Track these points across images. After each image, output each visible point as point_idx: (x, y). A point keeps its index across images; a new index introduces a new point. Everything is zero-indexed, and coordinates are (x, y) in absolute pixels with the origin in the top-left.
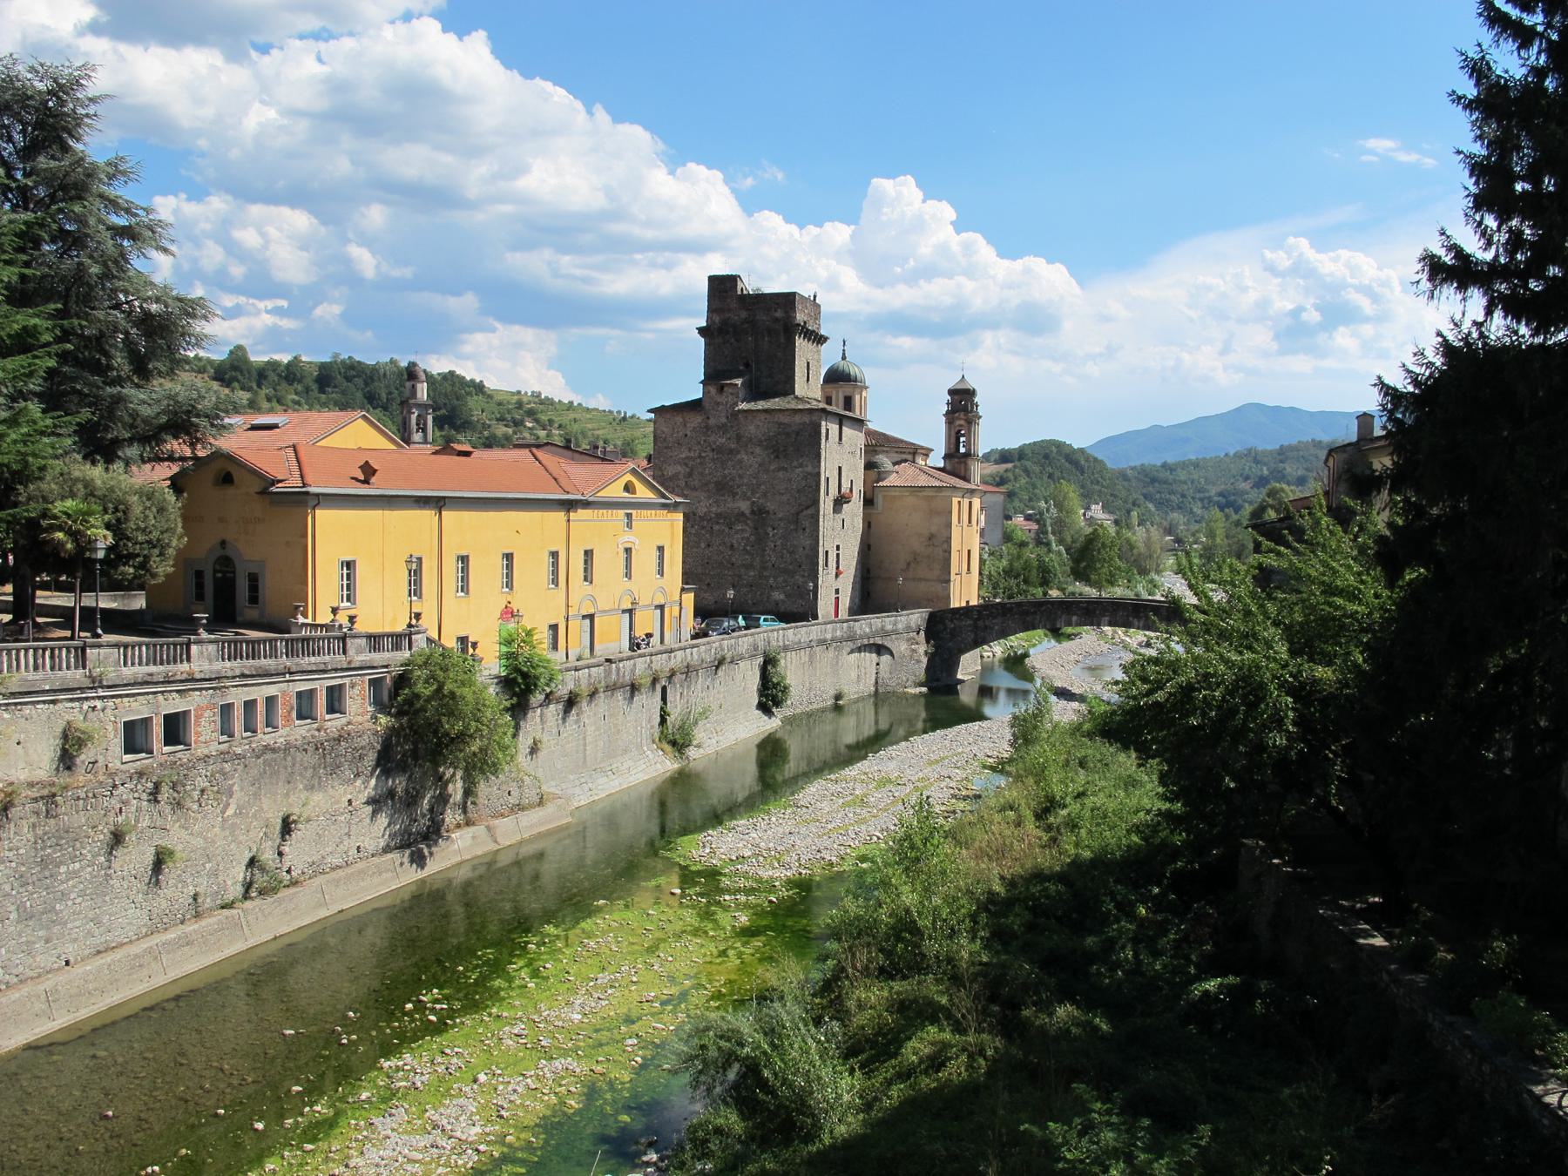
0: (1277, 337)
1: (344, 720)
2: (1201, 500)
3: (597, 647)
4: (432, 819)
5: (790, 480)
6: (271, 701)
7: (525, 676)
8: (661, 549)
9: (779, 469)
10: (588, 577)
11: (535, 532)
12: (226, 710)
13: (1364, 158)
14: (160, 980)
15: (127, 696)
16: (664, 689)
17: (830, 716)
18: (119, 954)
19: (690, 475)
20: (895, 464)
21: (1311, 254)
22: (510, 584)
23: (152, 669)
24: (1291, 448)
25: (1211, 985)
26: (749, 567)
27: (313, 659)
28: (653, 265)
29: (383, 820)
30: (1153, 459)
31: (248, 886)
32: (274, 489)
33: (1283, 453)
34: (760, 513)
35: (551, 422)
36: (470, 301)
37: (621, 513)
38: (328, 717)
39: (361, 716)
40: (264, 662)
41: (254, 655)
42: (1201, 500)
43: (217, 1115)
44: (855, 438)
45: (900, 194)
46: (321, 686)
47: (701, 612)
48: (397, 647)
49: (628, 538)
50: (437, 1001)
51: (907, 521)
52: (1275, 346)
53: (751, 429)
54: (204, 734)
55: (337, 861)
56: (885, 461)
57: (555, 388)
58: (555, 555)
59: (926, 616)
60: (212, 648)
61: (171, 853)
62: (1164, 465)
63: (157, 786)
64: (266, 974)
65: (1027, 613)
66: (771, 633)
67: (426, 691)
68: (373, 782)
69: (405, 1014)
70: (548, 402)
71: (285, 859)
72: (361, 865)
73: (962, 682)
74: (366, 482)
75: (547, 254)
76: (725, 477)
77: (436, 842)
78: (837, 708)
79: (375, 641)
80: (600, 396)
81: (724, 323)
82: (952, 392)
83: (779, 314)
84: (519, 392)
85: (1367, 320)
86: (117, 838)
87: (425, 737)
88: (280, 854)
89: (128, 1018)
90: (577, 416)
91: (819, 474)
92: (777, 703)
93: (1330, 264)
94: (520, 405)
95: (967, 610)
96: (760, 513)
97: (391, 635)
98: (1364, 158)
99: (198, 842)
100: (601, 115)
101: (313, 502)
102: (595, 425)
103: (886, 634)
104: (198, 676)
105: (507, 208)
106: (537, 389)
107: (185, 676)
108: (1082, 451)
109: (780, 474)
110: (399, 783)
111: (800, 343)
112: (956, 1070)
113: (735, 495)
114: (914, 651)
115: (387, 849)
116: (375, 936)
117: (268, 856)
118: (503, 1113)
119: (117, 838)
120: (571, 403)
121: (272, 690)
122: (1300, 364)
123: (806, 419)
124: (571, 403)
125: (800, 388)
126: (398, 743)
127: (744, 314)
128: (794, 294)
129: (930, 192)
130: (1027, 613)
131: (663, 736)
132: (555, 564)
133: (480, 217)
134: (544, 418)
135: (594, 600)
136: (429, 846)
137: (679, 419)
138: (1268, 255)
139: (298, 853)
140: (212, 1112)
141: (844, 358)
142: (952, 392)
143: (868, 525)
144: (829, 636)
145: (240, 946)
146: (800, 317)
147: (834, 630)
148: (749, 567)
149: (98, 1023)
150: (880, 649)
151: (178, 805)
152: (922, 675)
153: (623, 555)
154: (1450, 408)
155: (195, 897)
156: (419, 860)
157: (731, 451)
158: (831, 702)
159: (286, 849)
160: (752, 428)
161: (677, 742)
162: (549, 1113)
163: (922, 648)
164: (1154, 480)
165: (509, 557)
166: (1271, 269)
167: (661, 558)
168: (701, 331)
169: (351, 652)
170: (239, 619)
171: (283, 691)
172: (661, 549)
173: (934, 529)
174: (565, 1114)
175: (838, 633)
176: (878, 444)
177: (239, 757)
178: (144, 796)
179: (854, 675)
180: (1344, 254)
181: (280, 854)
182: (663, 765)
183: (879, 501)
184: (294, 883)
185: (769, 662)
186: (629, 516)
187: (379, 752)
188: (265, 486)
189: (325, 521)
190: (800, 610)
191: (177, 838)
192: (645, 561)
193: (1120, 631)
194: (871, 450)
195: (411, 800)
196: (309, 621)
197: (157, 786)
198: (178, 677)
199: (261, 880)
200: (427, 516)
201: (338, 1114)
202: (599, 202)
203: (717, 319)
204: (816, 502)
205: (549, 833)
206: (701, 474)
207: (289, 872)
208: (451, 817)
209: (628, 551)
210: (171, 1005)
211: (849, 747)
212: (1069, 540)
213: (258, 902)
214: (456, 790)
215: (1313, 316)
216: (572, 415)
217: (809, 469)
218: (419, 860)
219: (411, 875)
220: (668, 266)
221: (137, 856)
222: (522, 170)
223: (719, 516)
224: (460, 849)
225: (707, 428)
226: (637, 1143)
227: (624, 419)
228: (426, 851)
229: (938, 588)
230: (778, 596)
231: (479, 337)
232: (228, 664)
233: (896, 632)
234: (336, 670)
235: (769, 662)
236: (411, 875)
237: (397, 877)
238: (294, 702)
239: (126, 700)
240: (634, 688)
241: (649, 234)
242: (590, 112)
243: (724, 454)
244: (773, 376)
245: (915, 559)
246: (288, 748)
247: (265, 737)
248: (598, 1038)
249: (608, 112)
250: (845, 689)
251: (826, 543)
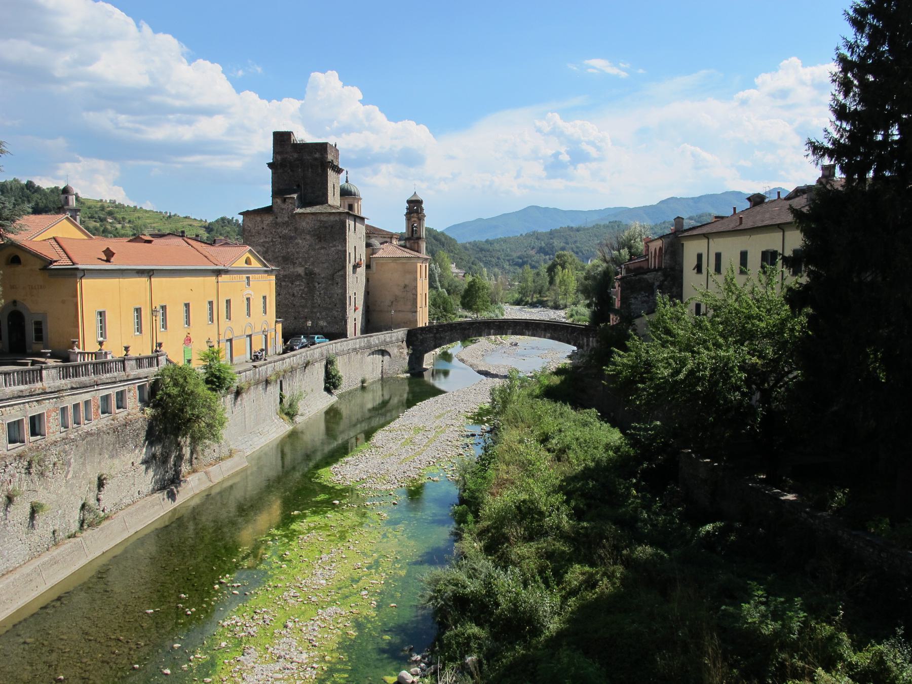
0: (546, 168)
1: (126, 413)
2: (508, 261)
3: (235, 358)
4: (175, 471)
5: (328, 255)
6: (87, 403)
7: (218, 378)
8: (265, 298)
10: (229, 317)
11: (200, 289)
12: (64, 410)
13: (590, 71)
14: (43, 589)
15: (9, 406)
16: (281, 382)
17: (359, 393)
18: (16, 575)
20: (381, 244)
21: (560, 123)
22: (188, 322)
23: (22, 387)
24: (556, 231)
25: (709, 527)
27: (108, 375)
28: (180, 122)
29: (151, 473)
30: (481, 238)
31: (82, 523)
32: (52, 267)
33: (552, 234)
34: (310, 274)
35: (123, 218)
36: (61, 142)
37: (245, 276)
38: (117, 411)
39: (135, 411)
40: (84, 379)
41: (76, 375)
42: (508, 261)
43: (134, 669)
44: (361, 229)
45: (328, 82)
46: (112, 392)
47: (286, 337)
48: (151, 365)
49: (248, 292)
50: (232, 581)
51: (391, 278)
52: (544, 174)
53: (304, 224)
54: (52, 428)
55: (127, 501)
56: (375, 242)
57: (120, 197)
58: (211, 303)
59: (406, 332)
60: (54, 371)
61: (42, 506)
62: (487, 241)
63: (30, 463)
64: (98, 580)
65: (465, 329)
66: (324, 347)
67: (174, 391)
68: (144, 450)
69: (217, 591)
70: (121, 207)
71: (102, 502)
72: (142, 502)
73: (426, 370)
74: (108, 261)
75: (111, 114)
76: (288, 253)
77: (179, 484)
78: (363, 388)
79: (139, 361)
80: (148, 202)
81: (284, 160)
82: (409, 202)
83: (317, 155)
84: (101, 201)
85: (595, 160)
86: (10, 499)
87: (173, 418)
88: (98, 500)
89: (33, 615)
90: (140, 215)
91: (345, 251)
92: (335, 387)
93: (575, 128)
94: (103, 208)
95: (422, 329)
96: (310, 274)
97: (147, 358)
98: (590, 71)
99: (53, 497)
100: (146, 28)
101: (80, 274)
102: (151, 221)
103: (387, 343)
104: (48, 390)
105: (81, 84)
106: (113, 198)
107: (41, 391)
108: (442, 233)
109: (322, 251)
110: (158, 449)
111: (331, 173)
112: (604, 586)
113: (294, 264)
114: (401, 353)
115: (154, 491)
116: (152, 548)
117: (92, 502)
118: (314, 643)
119: (10, 499)
120: (135, 207)
121: (87, 397)
122: (558, 184)
123: (337, 218)
124: (135, 207)
125: (331, 201)
126: (157, 425)
127: (296, 155)
128: (326, 144)
129: (346, 80)
130: (465, 329)
131: (282, 410)
132: (211, 309)
133: (65, 89)
134: (119, 216)
135: (232, 330)
136: (176, 487)
137: (259, 219)
138: (538, 123)
139: (108, 498)
140: (131, 667)
141: (347, 182)
142: (409, 202)
143: (368, 280)
144: (358, 346)
145: (83, 562)
146: (330, 157)
147: (360, 343)
148: (304, 307)
149: (16, 621)
150: (383, 353)
151: (42, 474)
152: (406, 367)
153: (262, 300)
154: (818, 211)
155: (54, 532)
156: (172, 496)
157: (291, 238)
158: (360, 385)
159: (101, 497)
160: (304, 224)
161: (290, 413)
162: (341, 640)
163: (405, 351)
164: (482, 250)
165: (187, 305)
166: (539, 130)
167: (265, 303)
168: (270, 165)
169: (128, 369)
170: (28, 351)
171: (94, 396)
172: (265, 298)
173: (407, 282)
174: (351, 640)
175: (362, 344)
176: (372, 232)
177: (73, 440)
178: (23, 471)
179: (370, 369)
180: (578, 122)
181: (98, 500)
182: (283, 428)
183: (374, 265)
184: (107, 518)
185: (329, 362)
186: (248, 278)
187: (147, 431)
188: (46, 264)
189: (87, 285)
190: (337, 333)
191: (41, 497)
192: (257, 305)
193: (499, 337)
194: (368, 236)
195: (165, 460)
196: (81, 350)
197: (30, 463)
198: (37, 392)
199: (89, 517)
200: (144, 280)
201: (212, 657)
202: (144, 81)
203: (279, 158)
204: (344, 267)
205: (237, 473)
206: (274, 252)
207: (103, 511)
208: (185, 468)
209: (248, 299)
210: (58, 604)
211: (370, 410)
212: (447, 285)
213: (89, 531)
214: (187, 451)
215: (565, 158)
216: (137, 215)
217: (340, 248)
218: (172, 496)
219: (169, 506)
220: (190, 123)
221: (21, 510)
222: (93, 59)
224: (193, 486)
225: (276, 224)
226: (403, 650)
227: (170, 217)
228: (175, 490)
229: (410, 316)
231: (69, 165)
232: (63, 381)
233: (391, 342)
234: (121, 381)
235: (329, 362)
236: (169, 506)
237: (160, 508)
238: (100, 403)
239: (8, 409)
240: (267, 382)
241: (178, 103)
242: (138, 26)
243: (288, 240)
244: (315, 194)
245: (396, 299)
246: (99, 433)
247: (85, 427)
248: (344, 591)
249: (151, 27)
250: (367, 377)
251: (350, 292)
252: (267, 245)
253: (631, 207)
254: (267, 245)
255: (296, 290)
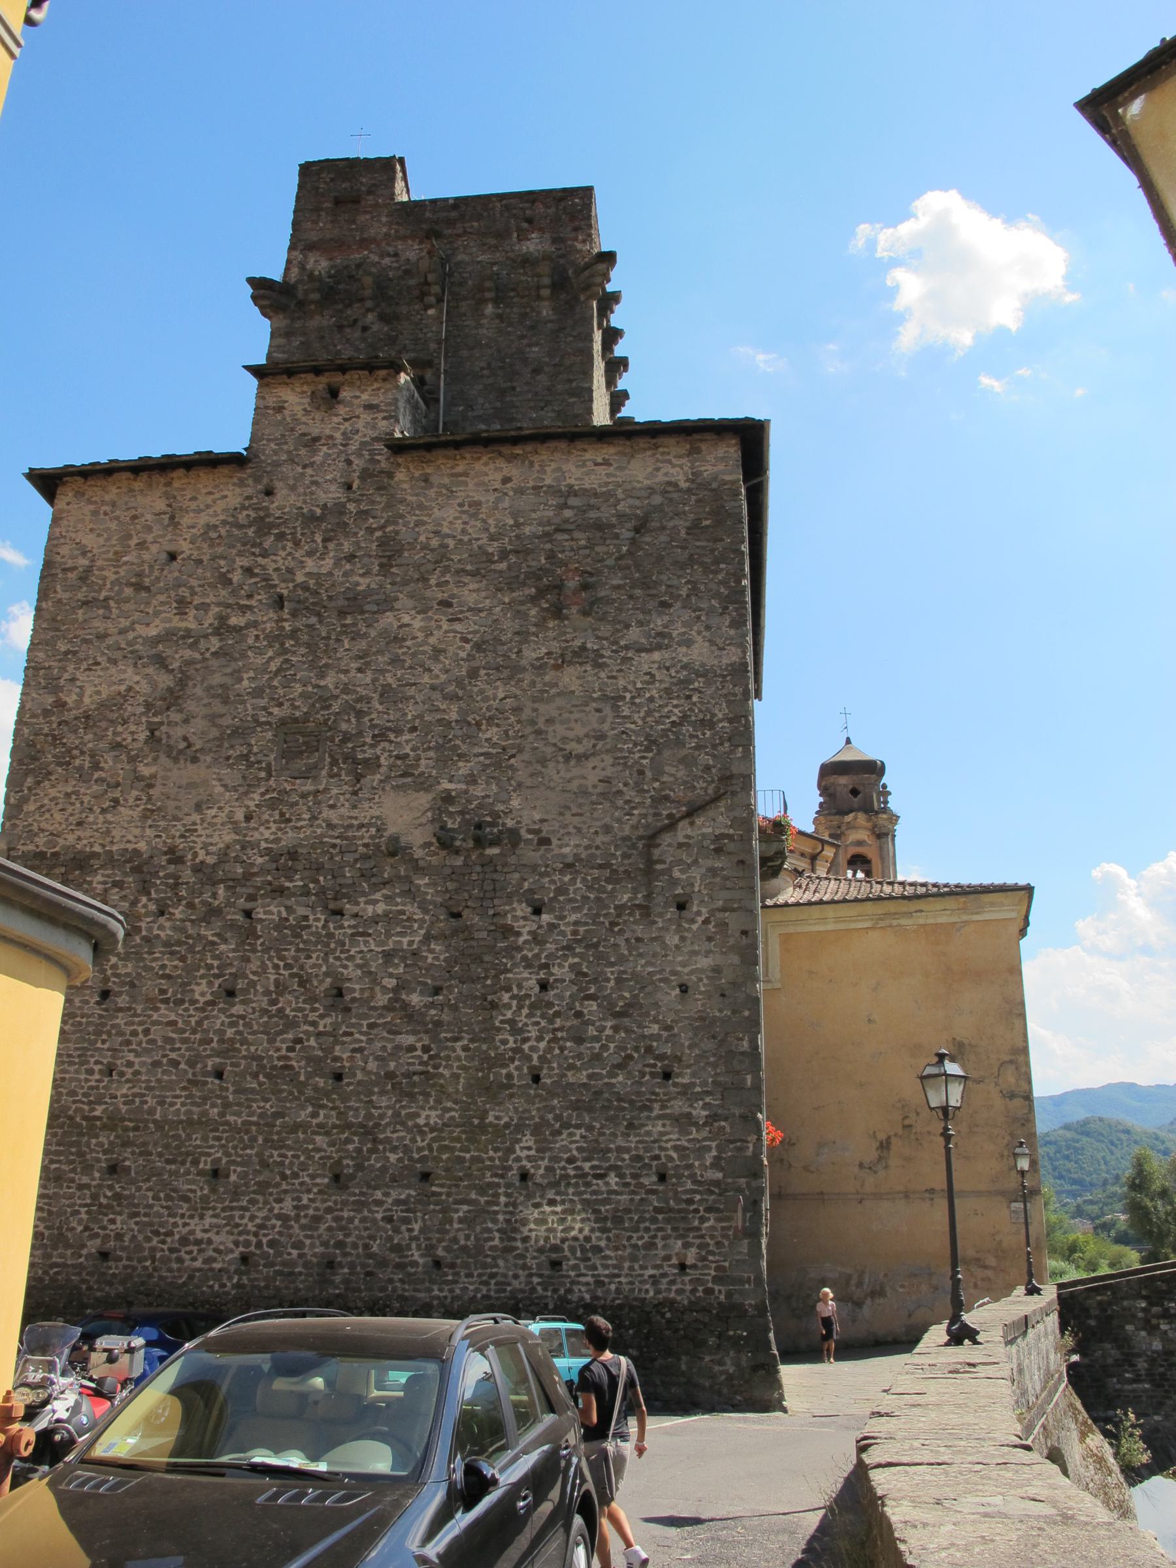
9: (563, 661)
19: (172, 699)
26: (406, 1087)
34: (474, 840)
59: (1048, 1348)
83: (534, 245)
96: (474, 840)
109: (570, 678)
113: (360, 768)
148: (406, 1087)
157: (354, 603)
223: (287, 859)
225: (263, 525)
230: (550, 1222)
252: (179, 656)
253: (1096, 1085)
254: (179, 656)
255: (358, 962)
